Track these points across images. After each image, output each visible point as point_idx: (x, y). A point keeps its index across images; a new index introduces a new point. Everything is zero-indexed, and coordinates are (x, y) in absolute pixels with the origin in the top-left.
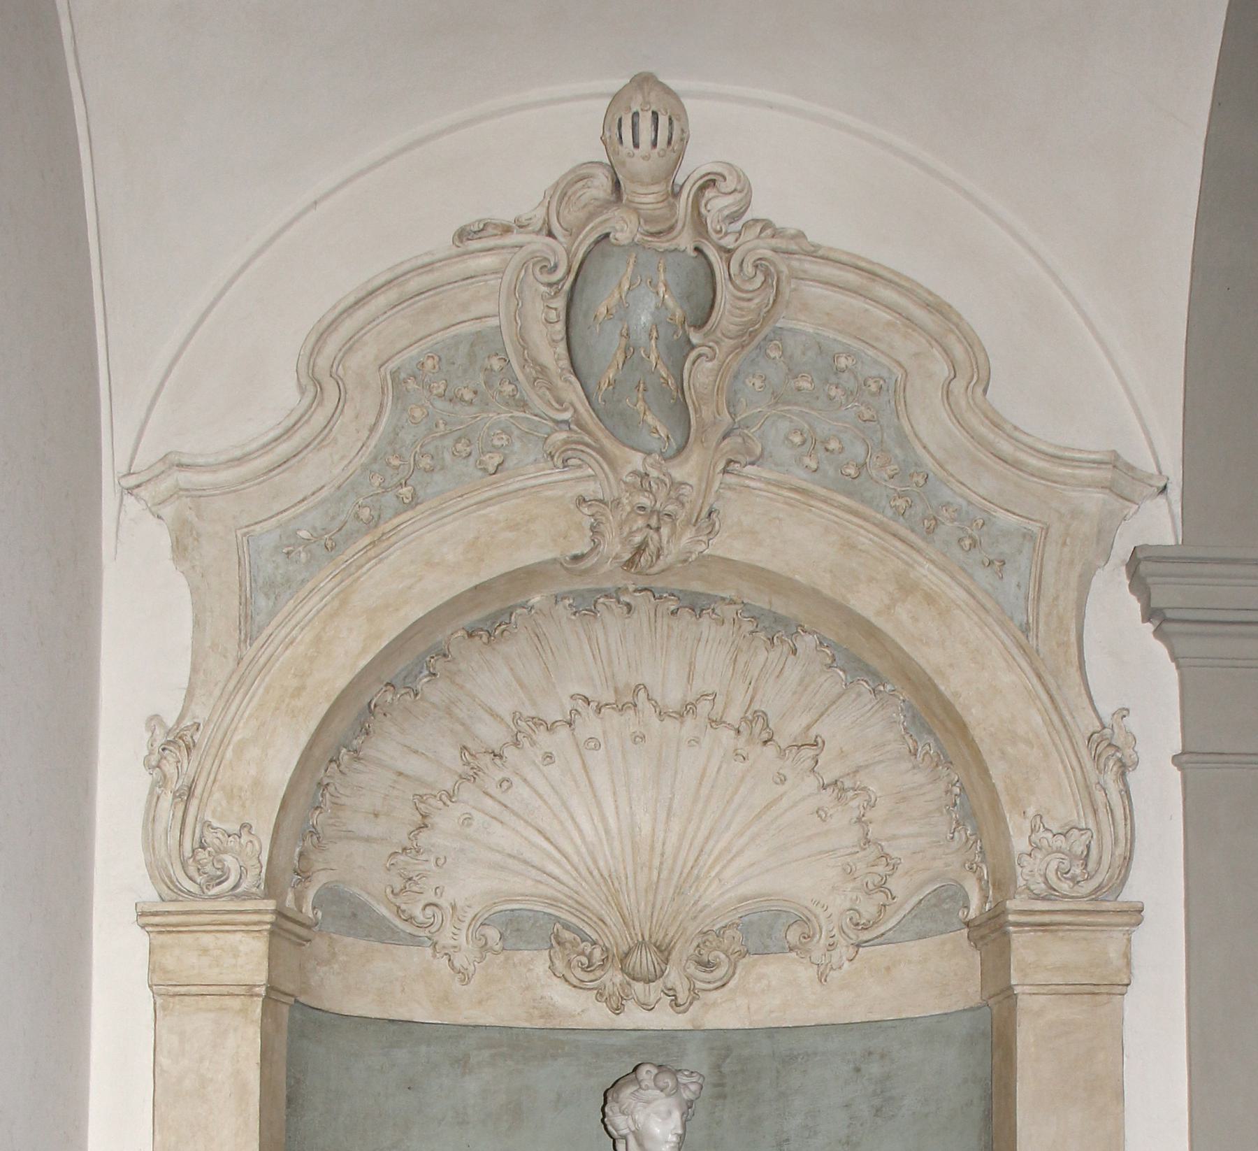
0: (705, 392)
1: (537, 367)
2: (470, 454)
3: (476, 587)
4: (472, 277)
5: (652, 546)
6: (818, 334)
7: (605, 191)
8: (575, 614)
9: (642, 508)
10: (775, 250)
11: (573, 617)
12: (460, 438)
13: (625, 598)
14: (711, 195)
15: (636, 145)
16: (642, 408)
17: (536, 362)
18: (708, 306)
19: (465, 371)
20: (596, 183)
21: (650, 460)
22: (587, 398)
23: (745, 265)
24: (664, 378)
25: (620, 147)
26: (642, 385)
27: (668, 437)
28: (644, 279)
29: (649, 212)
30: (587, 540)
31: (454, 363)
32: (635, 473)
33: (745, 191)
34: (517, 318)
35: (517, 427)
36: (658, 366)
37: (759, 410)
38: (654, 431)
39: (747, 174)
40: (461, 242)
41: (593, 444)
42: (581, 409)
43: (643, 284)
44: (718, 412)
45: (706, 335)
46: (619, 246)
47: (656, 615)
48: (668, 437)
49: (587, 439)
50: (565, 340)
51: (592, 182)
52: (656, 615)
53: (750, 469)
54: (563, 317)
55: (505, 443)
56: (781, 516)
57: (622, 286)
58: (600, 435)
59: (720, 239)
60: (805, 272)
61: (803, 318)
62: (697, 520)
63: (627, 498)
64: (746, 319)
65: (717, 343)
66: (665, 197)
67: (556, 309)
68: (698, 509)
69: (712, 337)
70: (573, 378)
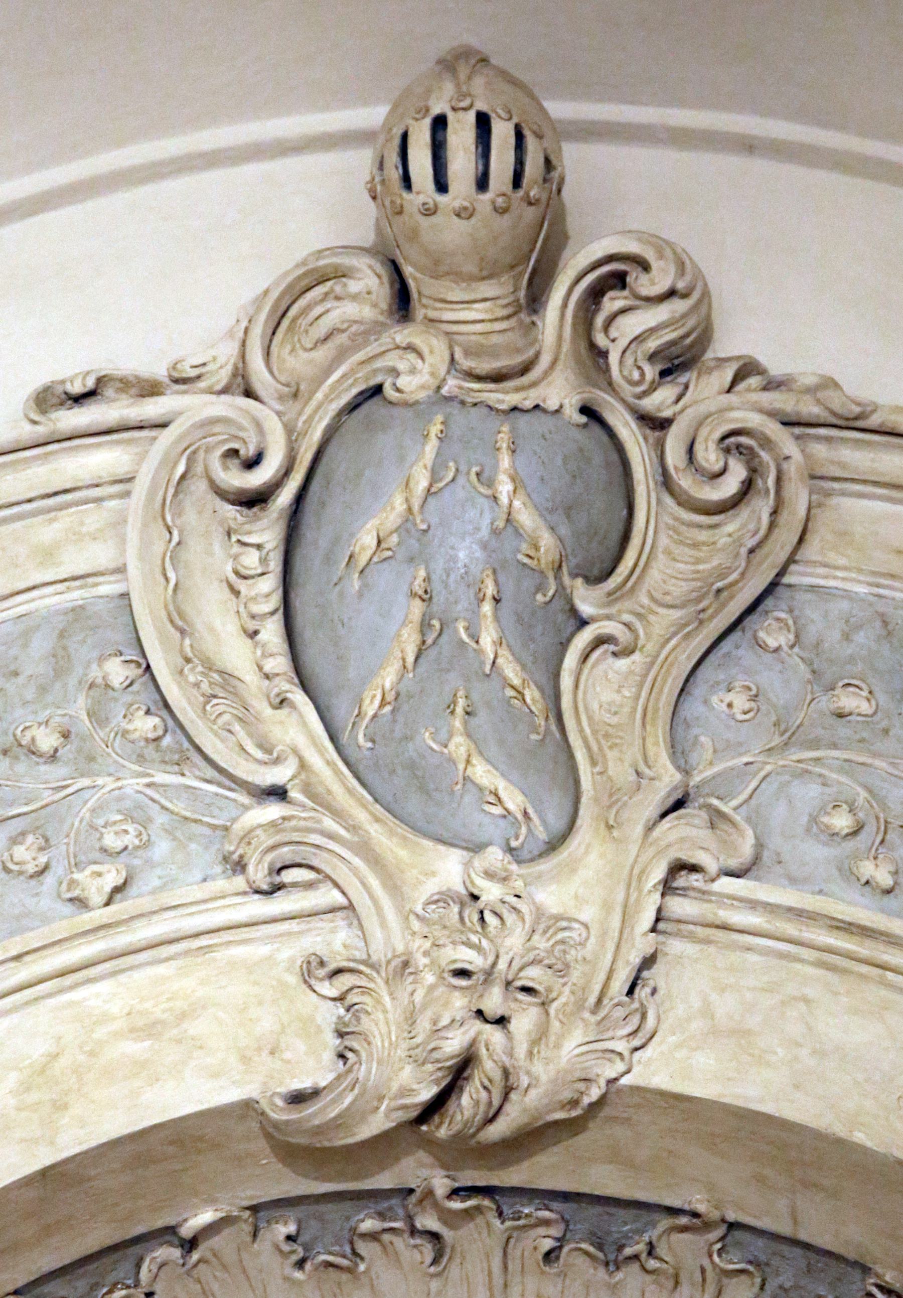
0: (614, 720)
1: (216, 676)
2: (46, 868)
3: (44, 1173)
4: (66, 491)
5: (488, 1065)
6: (880, 596)
7: (375, 305)
8: (300, 1264)
9: (463, 973)
10: (772, 414)
11: (298, 1275)
12: (23, 834)
13: (428, 1221)
14: (619, 304)
15: (442, 186)
16: (463, 750)
17: (209, 666)
18: (615, 537)
19: (43, 690)
20: (354, 286)
21: (479, 863)
22: (333, 738)
23: (699, 448)
24: (513, 687)
25: (405, 194)
26: (461, 703)
27: (526, 814)
28: (463, 468)
29: (473, 338)
30: (328, 1056)
31: (16, 674)
32: (443, 899)
33: (696, 296)
34: (167, 559)
35: (163, 807)
36: (500, 661)
37: (746, 759)
38: (492, 799)
39: (696, 258)
40: (44, 412)
41: (342, 832)
42: (315, 761)
43: (461, 480)
44: (646, 761)
45: (613, 597)
46: (406, 404)
47: (505, 1267)
48: (526, 814)
49: (329, 823)
50: (279, 615)
51: (345, 285)
52: (505, 1267)
53: (726, 884)
54: (275, 564)
55: (130, 840)
56: (810, 992)
57: (412, 485)
58: (361, 816)
59: (640, 396)
60: (843, 465)
61: (842, 561)
62: (599, 1001)
63: (426, 954)
64: (707, 566)
65: (639, 616)
66: (509, 311)
67: (259, 547)
68: (601, 977)
69: (627, 604)
70: (299, 697)
